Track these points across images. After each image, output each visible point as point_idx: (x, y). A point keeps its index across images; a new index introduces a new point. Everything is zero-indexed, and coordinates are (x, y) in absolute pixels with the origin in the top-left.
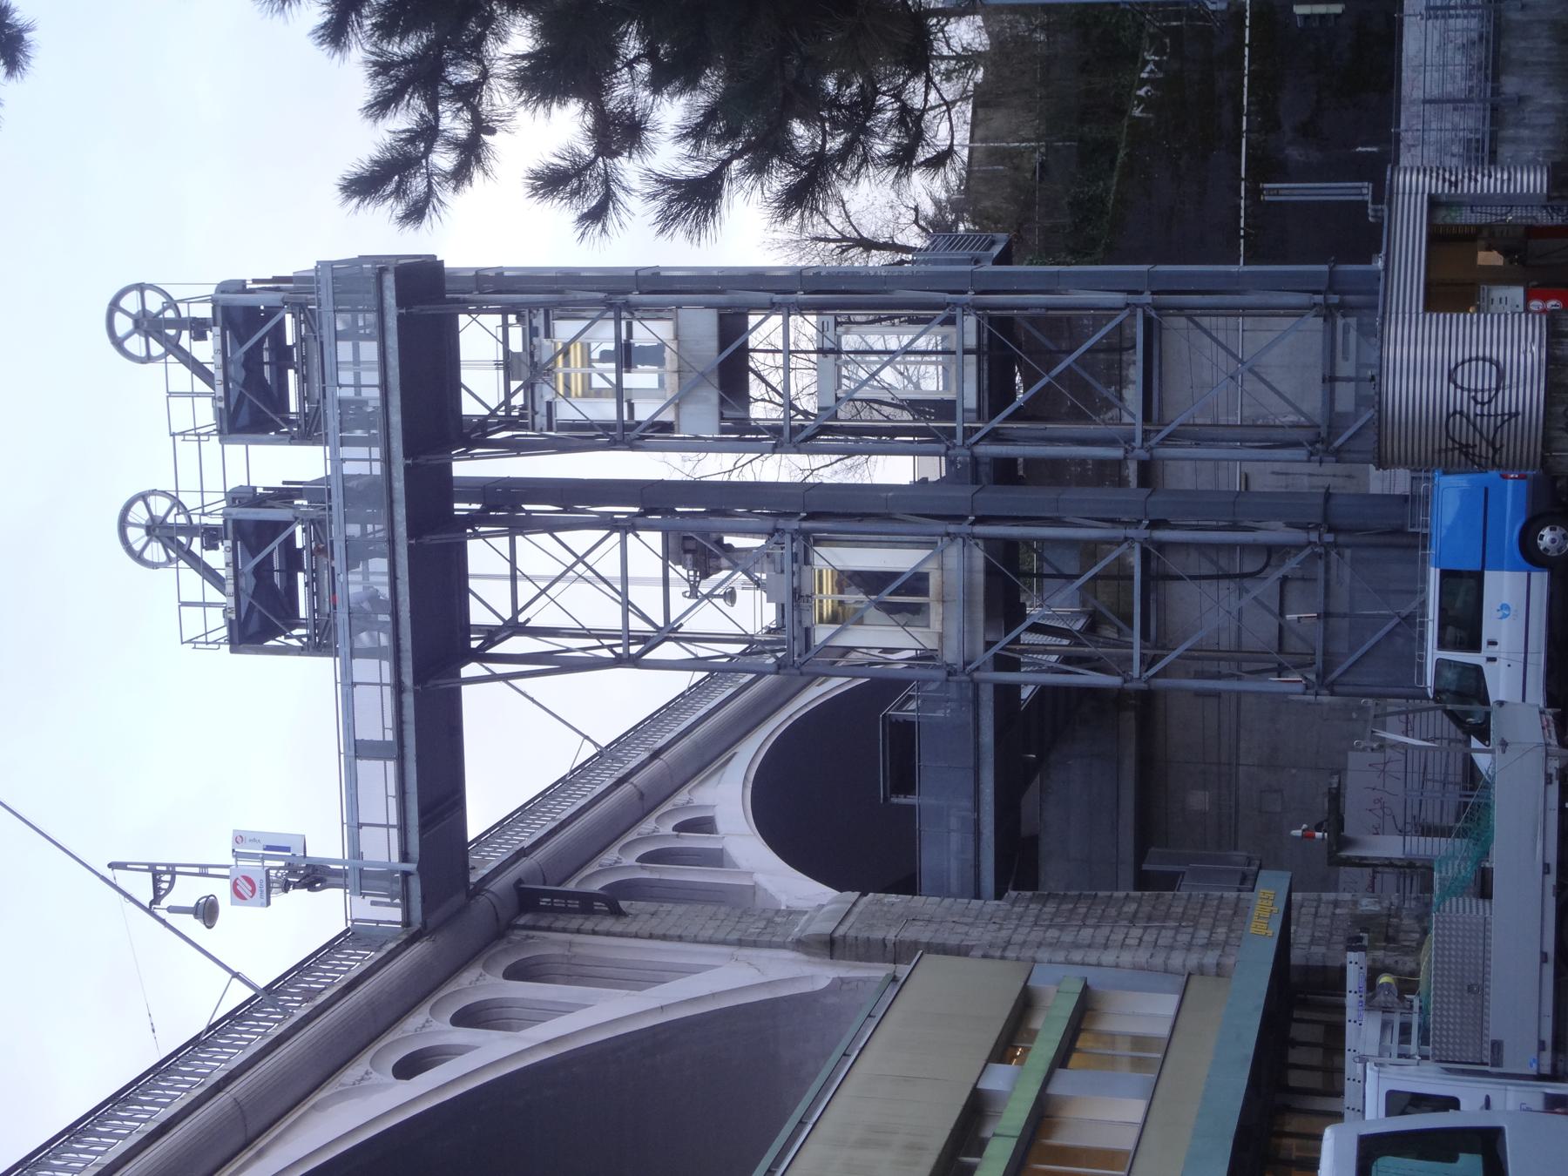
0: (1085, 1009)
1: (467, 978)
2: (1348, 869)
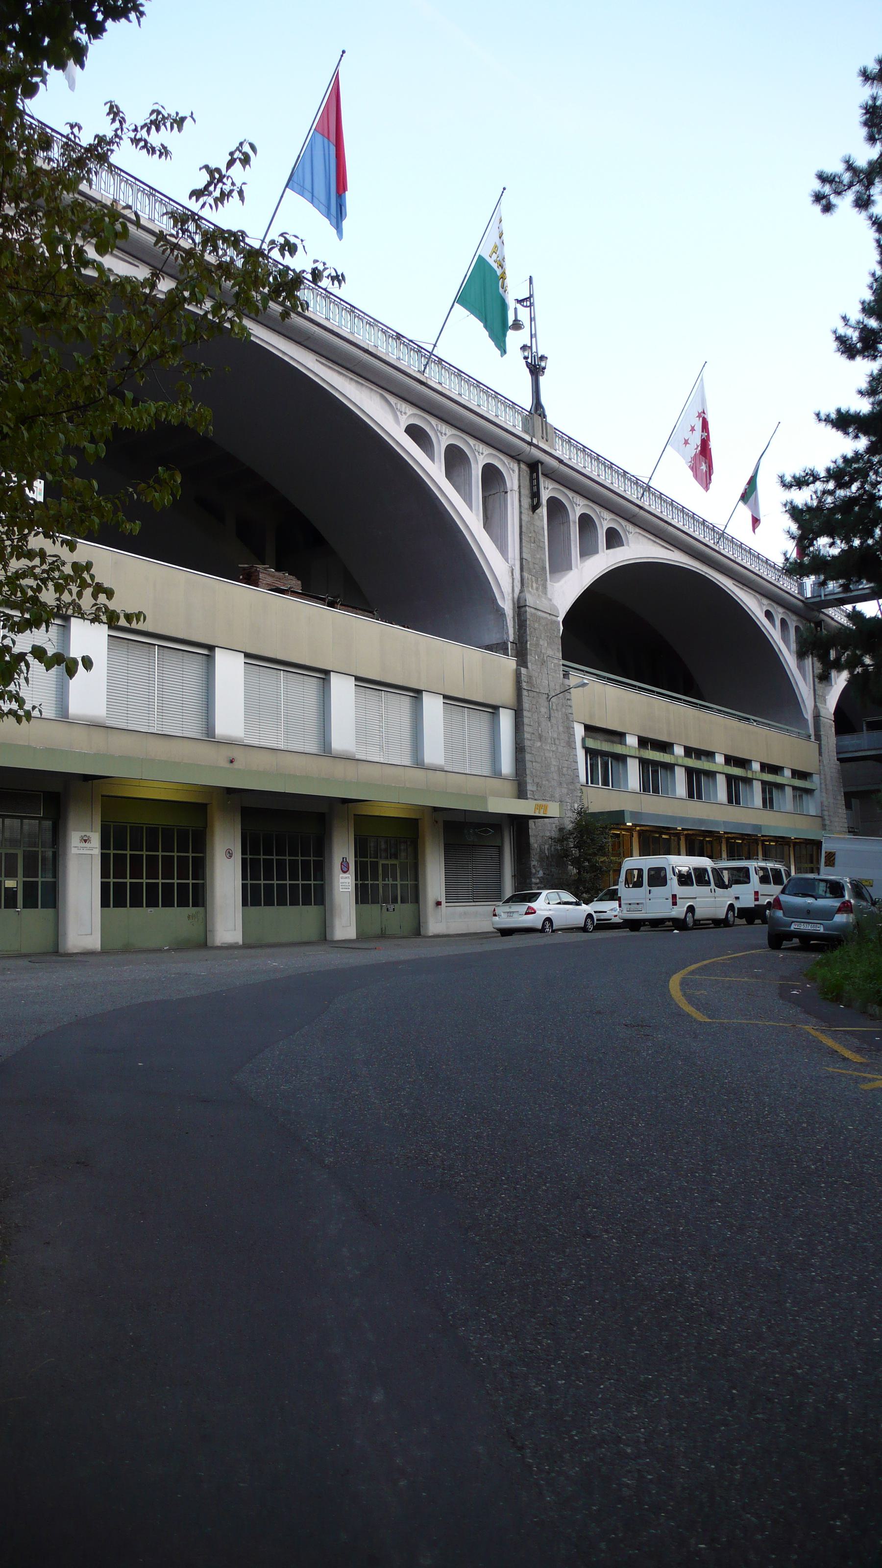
0: (809, 792)
1: (794, 618)
2: (96, 781)
